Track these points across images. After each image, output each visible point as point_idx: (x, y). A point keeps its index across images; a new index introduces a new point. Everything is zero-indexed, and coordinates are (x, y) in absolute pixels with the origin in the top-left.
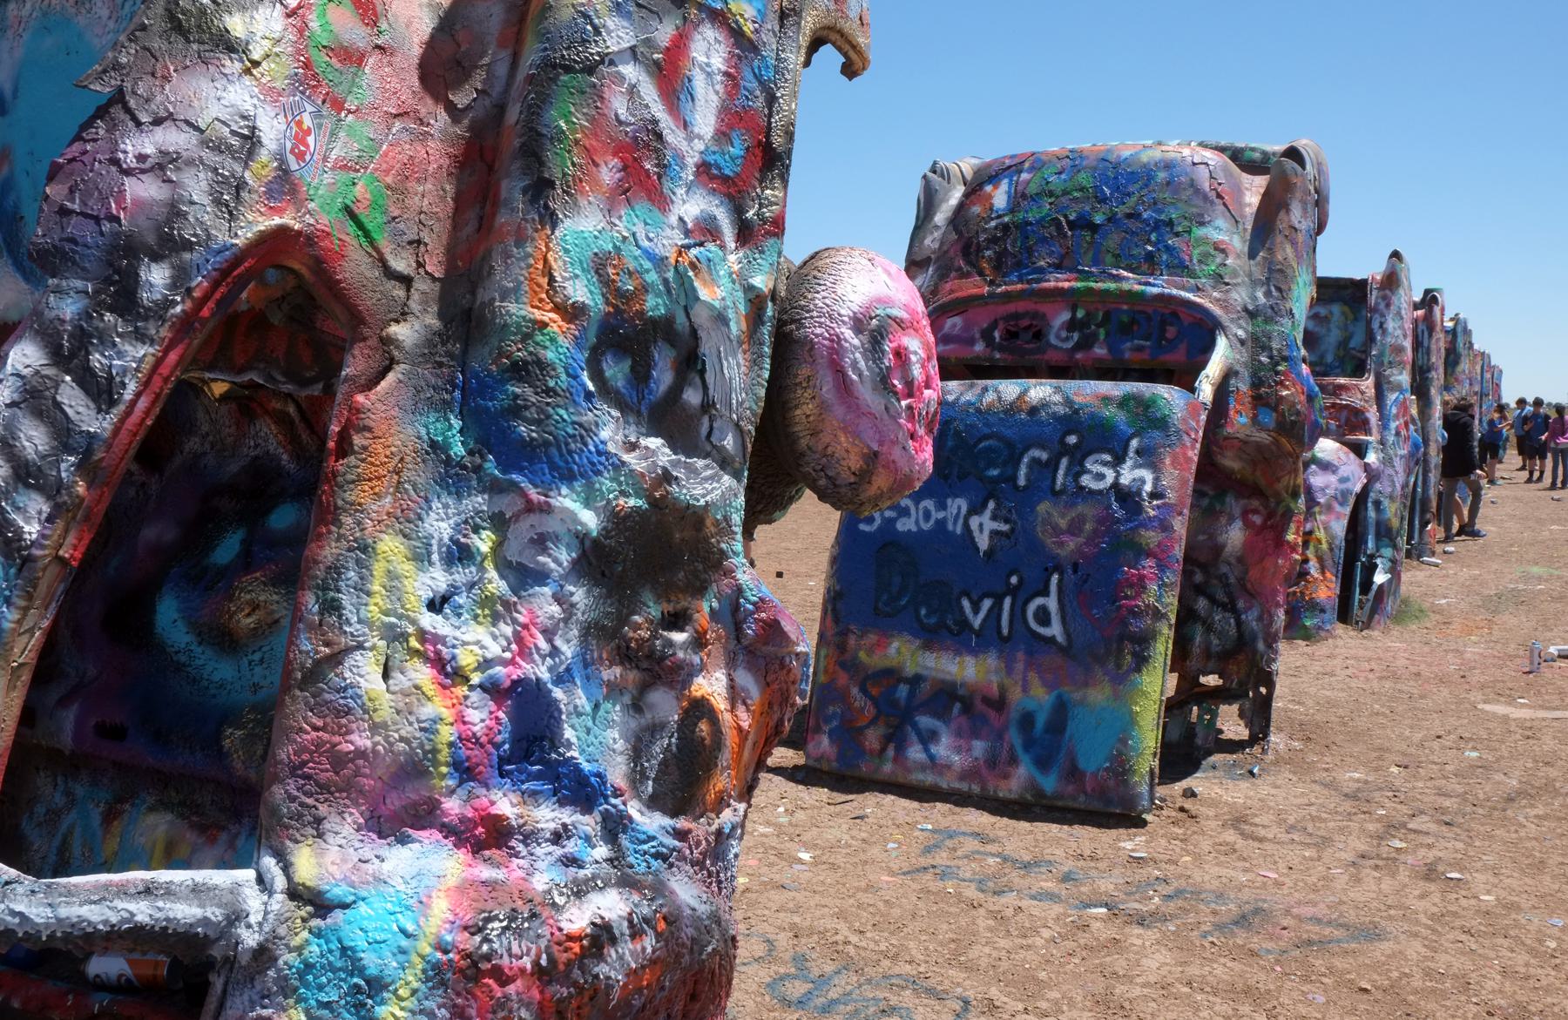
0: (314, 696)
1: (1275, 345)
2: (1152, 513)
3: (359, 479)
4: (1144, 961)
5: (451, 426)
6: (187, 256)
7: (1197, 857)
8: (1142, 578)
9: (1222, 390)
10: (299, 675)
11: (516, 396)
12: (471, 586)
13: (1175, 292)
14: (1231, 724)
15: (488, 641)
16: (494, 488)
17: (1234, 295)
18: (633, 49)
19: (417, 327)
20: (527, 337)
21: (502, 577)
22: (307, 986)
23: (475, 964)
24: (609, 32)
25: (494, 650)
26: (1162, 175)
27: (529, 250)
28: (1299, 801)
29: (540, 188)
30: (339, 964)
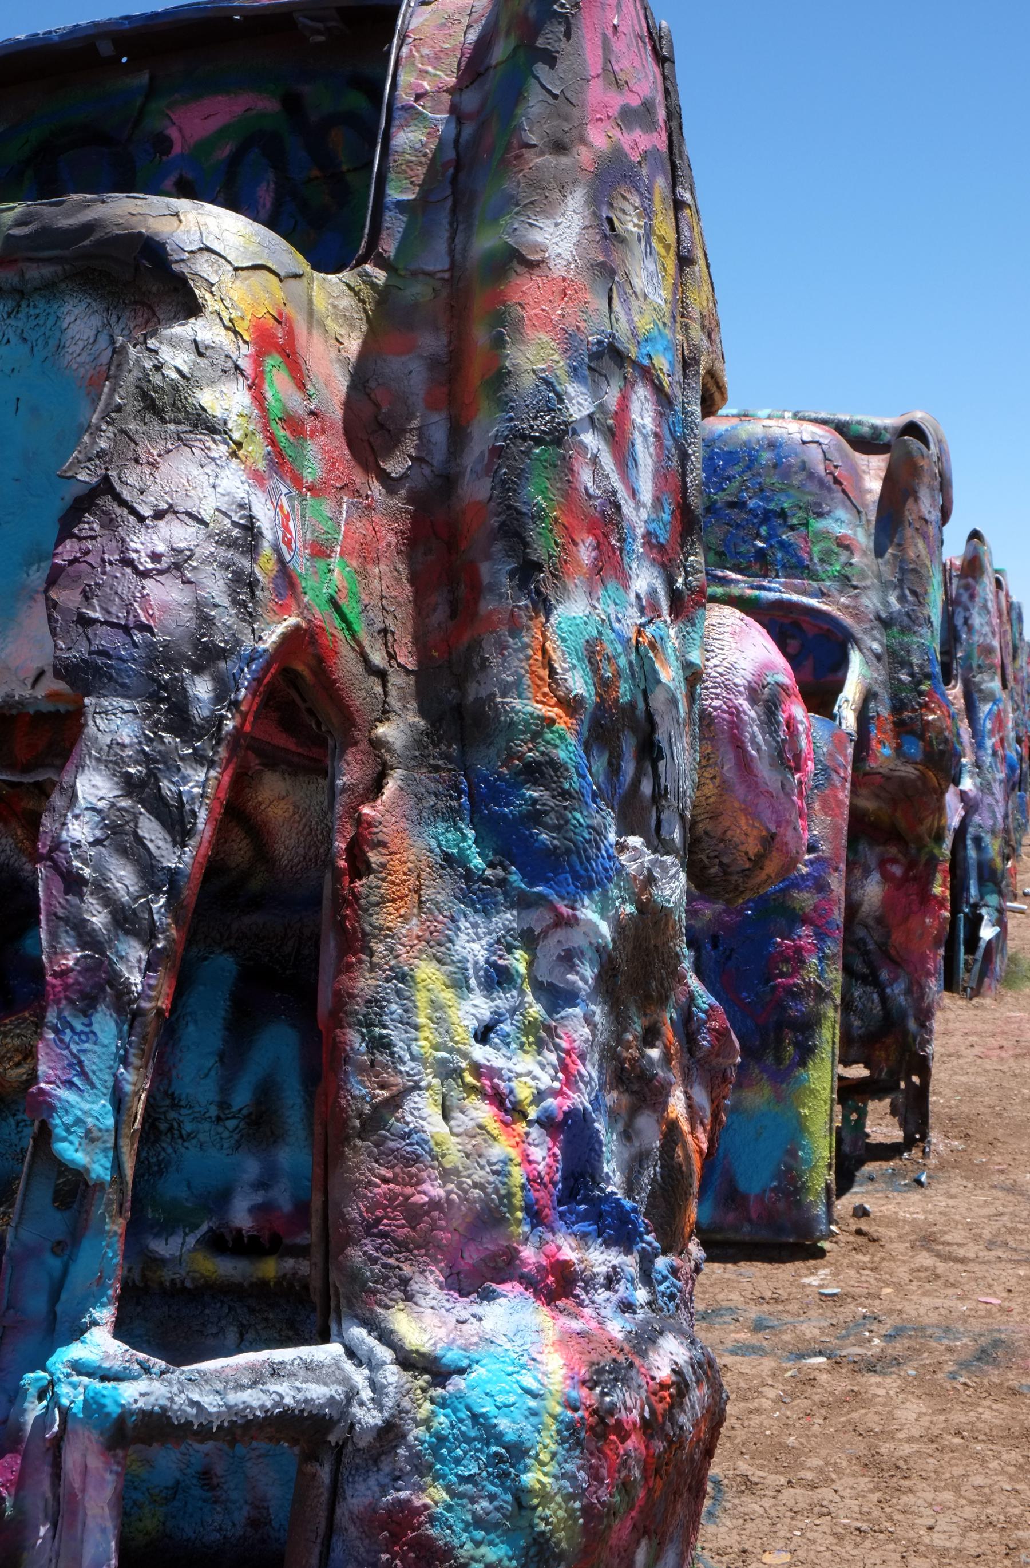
0: (377, 1146)
1: (915, 660)
2: (805, 870)
3: (383, 900)
4: (898, 1413)
5: (464, 837)
6: (222, 665)
7: (898, 1287)
8: (798, 950)
9: (863, 717)
10: (357, 1123)
11: (535, 801)
12: (513, 1011)
13: (795, 597)
14: (882, 1126)
15: (537, 1071)
16: (523, 903)
17: (865, 601)
18: (590, 417)
19: (402, 727)
20: (536, 735)
21: (538, 1000)
22: (443, 1461)
23: (602, 1420)
24: (570, 400)
25: (545, 1081)
26: (766, 456)
27: (526, 639)
28: (985, 1211)
29: (527, 571)
30: (473, 1434)
